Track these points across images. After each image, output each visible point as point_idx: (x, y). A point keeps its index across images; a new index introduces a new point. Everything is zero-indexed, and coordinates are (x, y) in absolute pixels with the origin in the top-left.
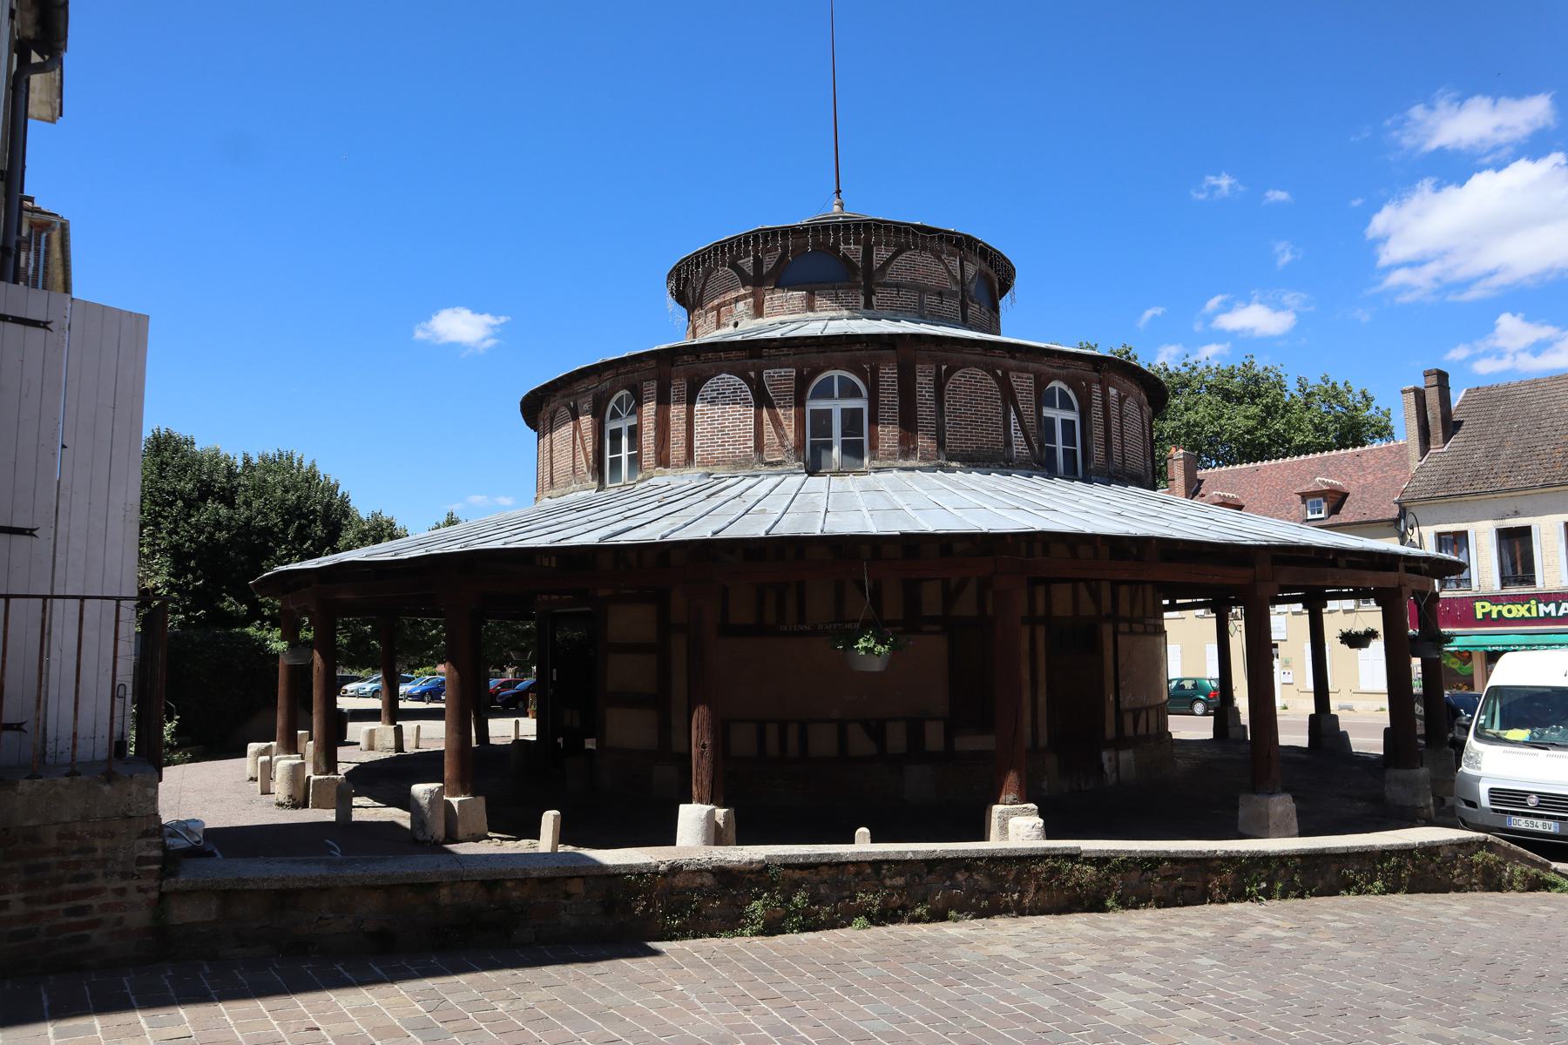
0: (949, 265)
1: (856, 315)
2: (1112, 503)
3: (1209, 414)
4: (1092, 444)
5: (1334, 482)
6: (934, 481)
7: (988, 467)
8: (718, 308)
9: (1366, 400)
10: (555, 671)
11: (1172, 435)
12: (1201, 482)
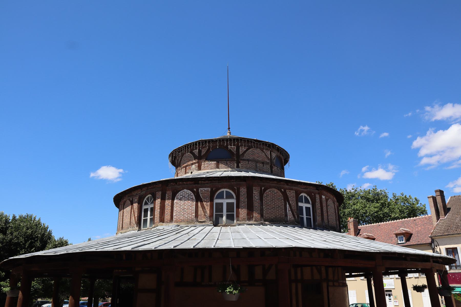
0: (266, 153)
1: (233, 170)
2: (323, 237)
3: (361, 206)
4: (317, 216)
5: (407, 230)
6: (259, 229)
7: (279, 224)
8: (186, 167)
9: (417, 201)
10: (118, 299)
11: (349, 214)
12: (360, 230)
